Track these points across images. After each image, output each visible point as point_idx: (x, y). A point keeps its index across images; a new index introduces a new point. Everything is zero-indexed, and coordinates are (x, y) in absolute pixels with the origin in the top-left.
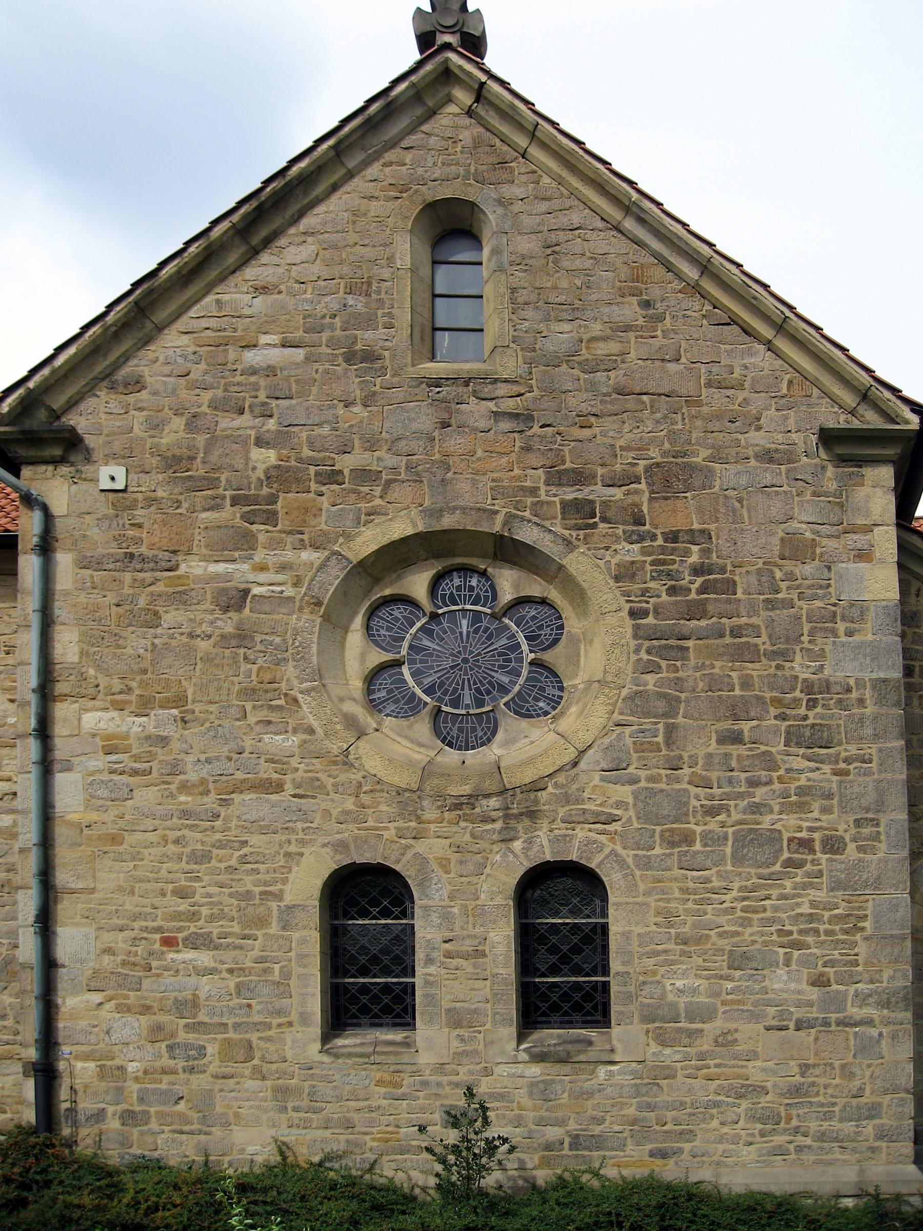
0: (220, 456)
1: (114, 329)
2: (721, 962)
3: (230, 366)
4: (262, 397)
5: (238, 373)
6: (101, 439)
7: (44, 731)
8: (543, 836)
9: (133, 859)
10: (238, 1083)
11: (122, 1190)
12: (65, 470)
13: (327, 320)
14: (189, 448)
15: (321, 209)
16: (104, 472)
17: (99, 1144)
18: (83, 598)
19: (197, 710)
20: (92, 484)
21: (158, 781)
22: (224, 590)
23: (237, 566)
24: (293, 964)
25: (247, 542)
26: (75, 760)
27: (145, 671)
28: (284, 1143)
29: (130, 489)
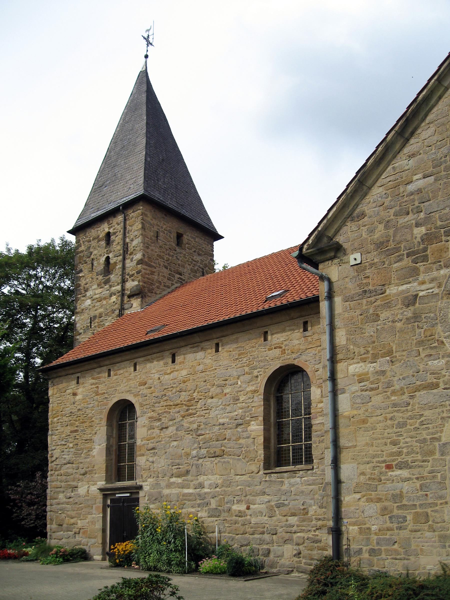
0: (400, 236)
1: (351, 194)
3: (401, 195)
4: (417, 204)
5: (405, 196)
6: (350, 243)
7: (333, 378)
9: (372, 429)
10: (422, 534)
11: (367, 588)
12: (336, 261)
13: (443, 159)
14: (386, 237)
15: (435, 109)
16: (352, 257)
17: (359, 565)
18: (346, 315)
19: (398, 356)
20: (347, 264)
21: (382, 392)
22: (406, 298)
23: (412, 285)
24: (447, 472)
25: (414, 273)
26: (346, 388)
27: (374, 342)
28: (445, 564)
29: (363, 262)
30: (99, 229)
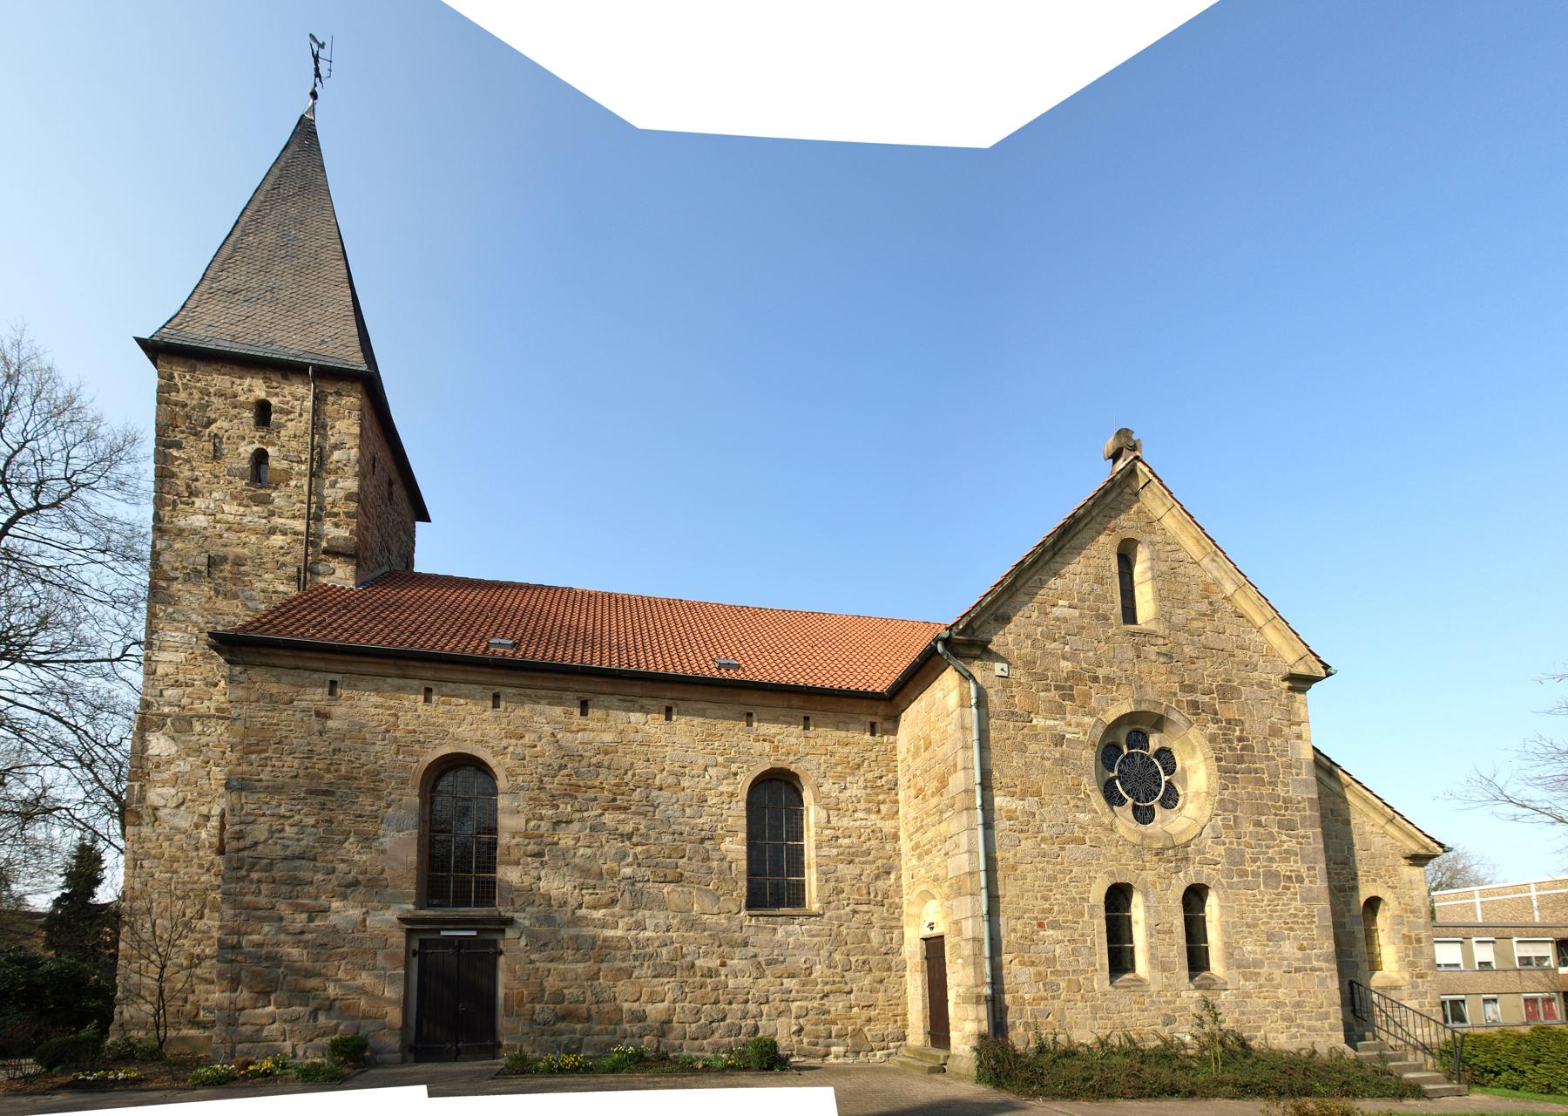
8: (1191, 870)
25: (1061, 710)
30: (238, 381)
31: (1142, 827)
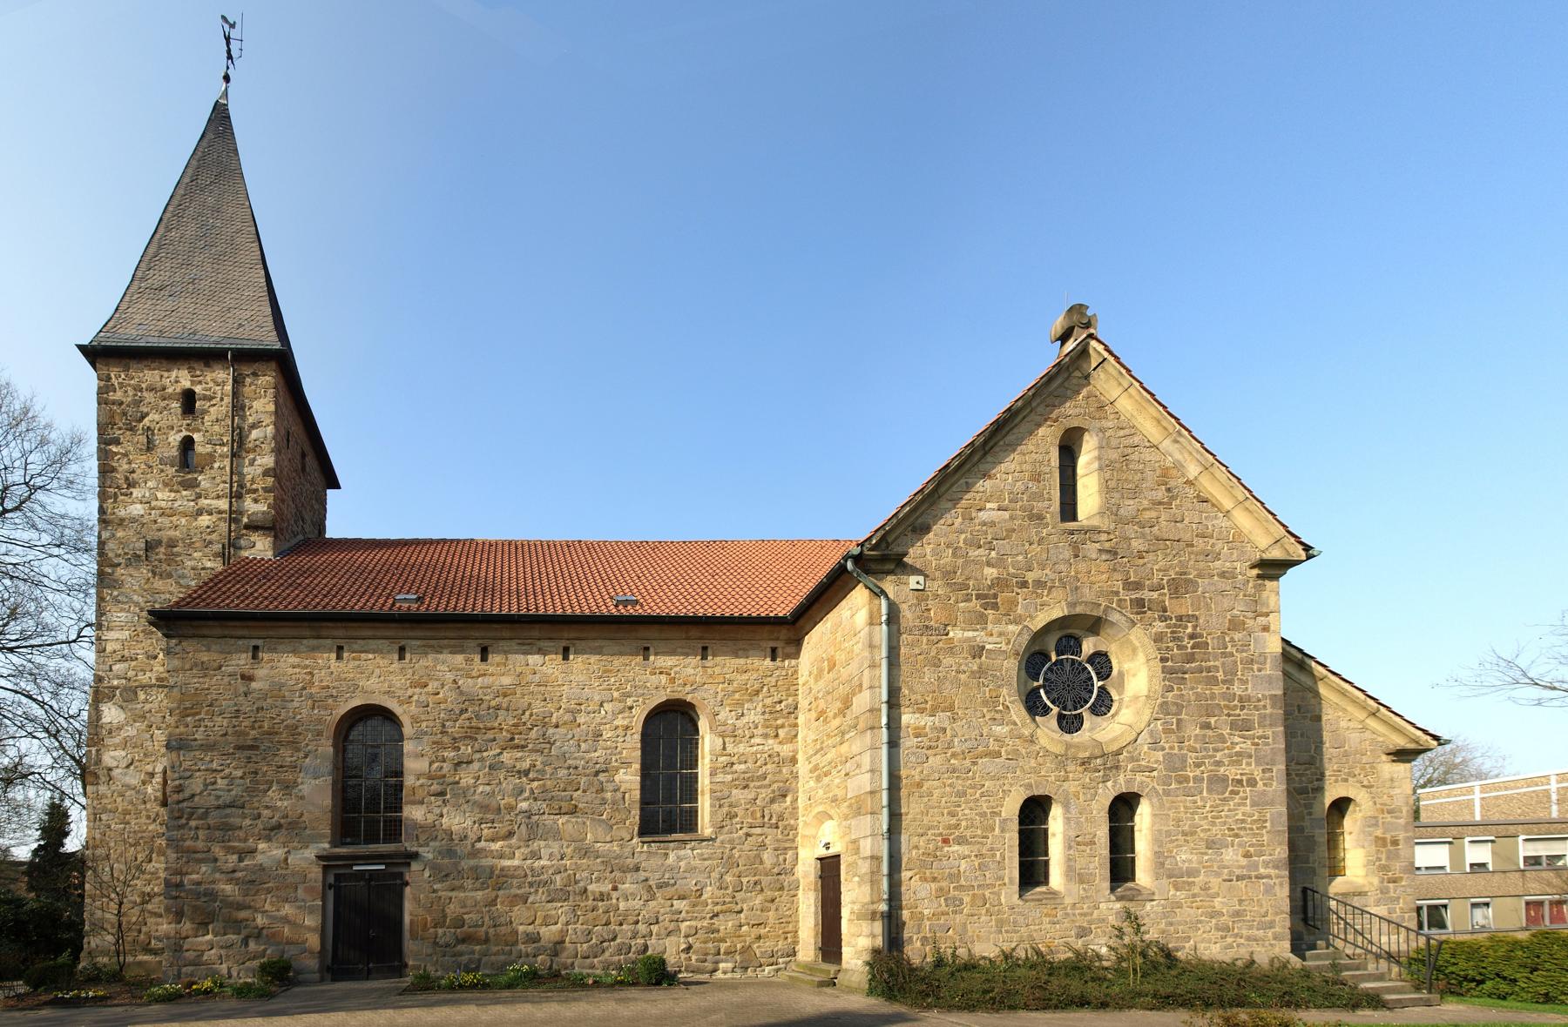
2: (1203, 844)
8: (1121, 779)
25: (982, 620)
31: (1067, 737)
